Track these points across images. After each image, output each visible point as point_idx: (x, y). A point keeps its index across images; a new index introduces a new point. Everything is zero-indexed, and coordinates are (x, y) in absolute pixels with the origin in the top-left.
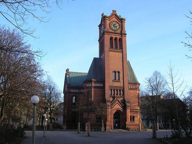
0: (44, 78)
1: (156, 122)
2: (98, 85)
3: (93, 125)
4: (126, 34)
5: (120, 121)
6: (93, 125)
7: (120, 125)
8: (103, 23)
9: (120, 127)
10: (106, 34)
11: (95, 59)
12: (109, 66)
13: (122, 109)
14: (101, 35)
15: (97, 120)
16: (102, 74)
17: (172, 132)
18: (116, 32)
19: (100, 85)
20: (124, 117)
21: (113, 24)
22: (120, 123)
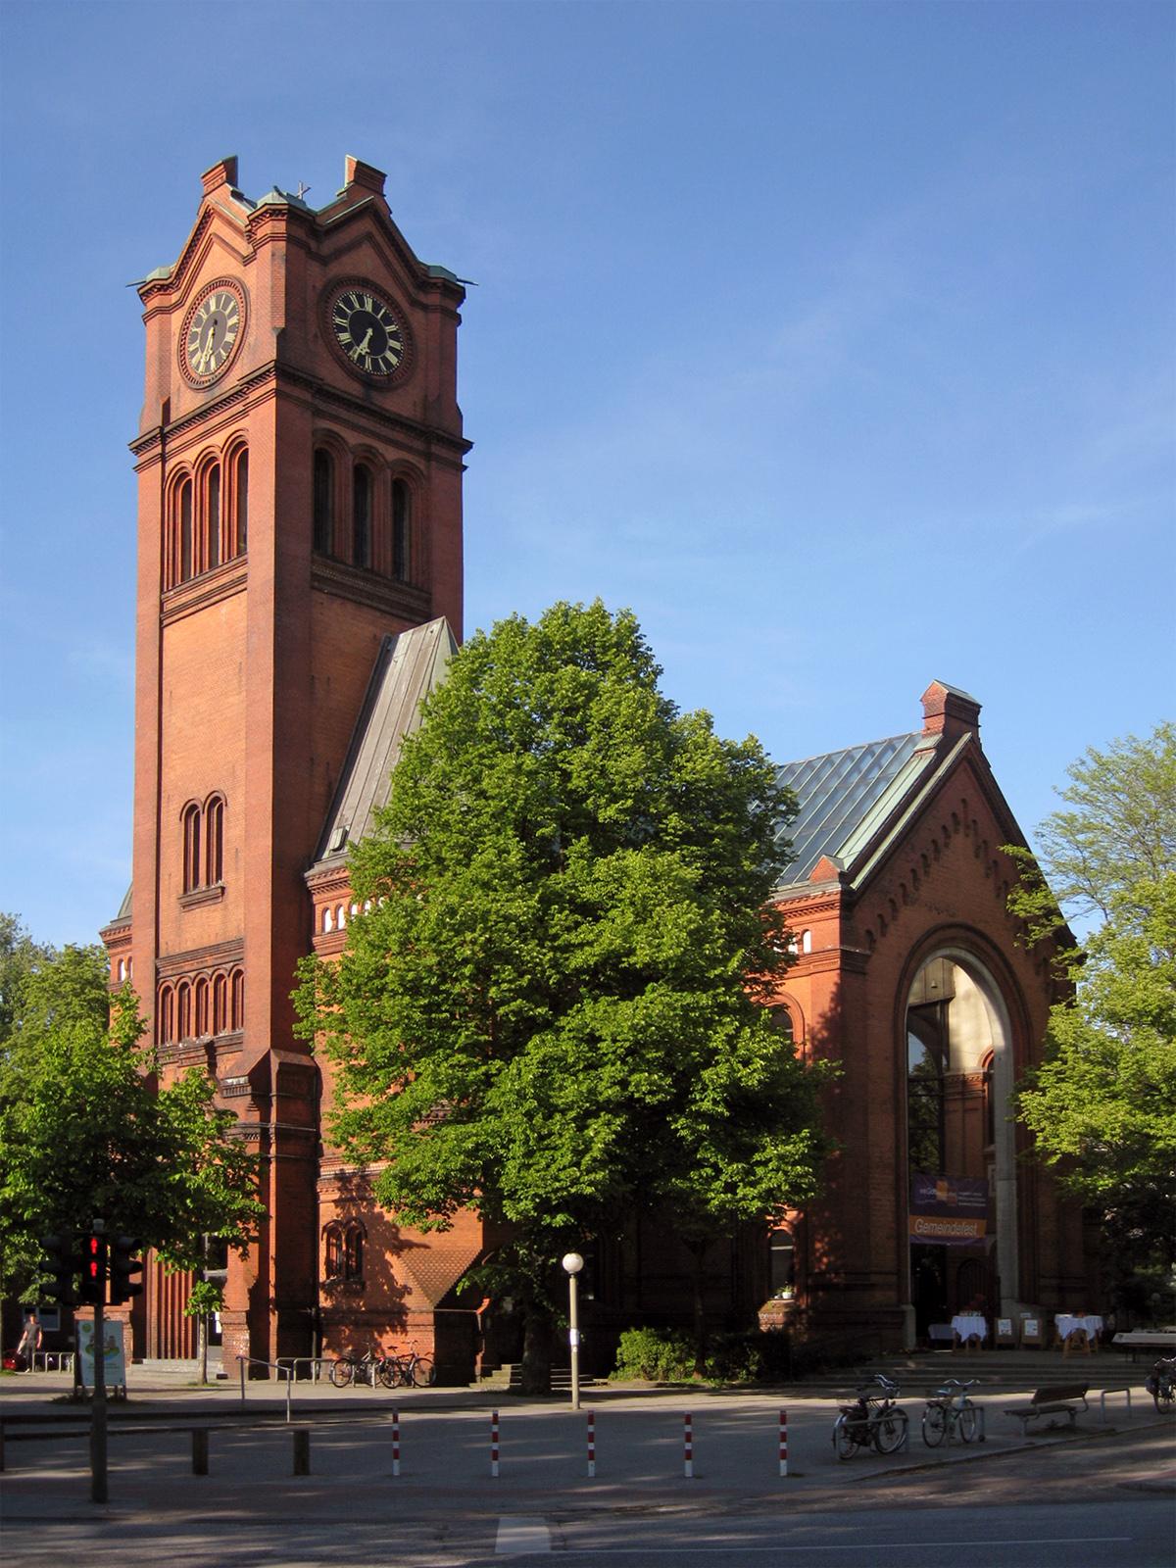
21: (350, 305)
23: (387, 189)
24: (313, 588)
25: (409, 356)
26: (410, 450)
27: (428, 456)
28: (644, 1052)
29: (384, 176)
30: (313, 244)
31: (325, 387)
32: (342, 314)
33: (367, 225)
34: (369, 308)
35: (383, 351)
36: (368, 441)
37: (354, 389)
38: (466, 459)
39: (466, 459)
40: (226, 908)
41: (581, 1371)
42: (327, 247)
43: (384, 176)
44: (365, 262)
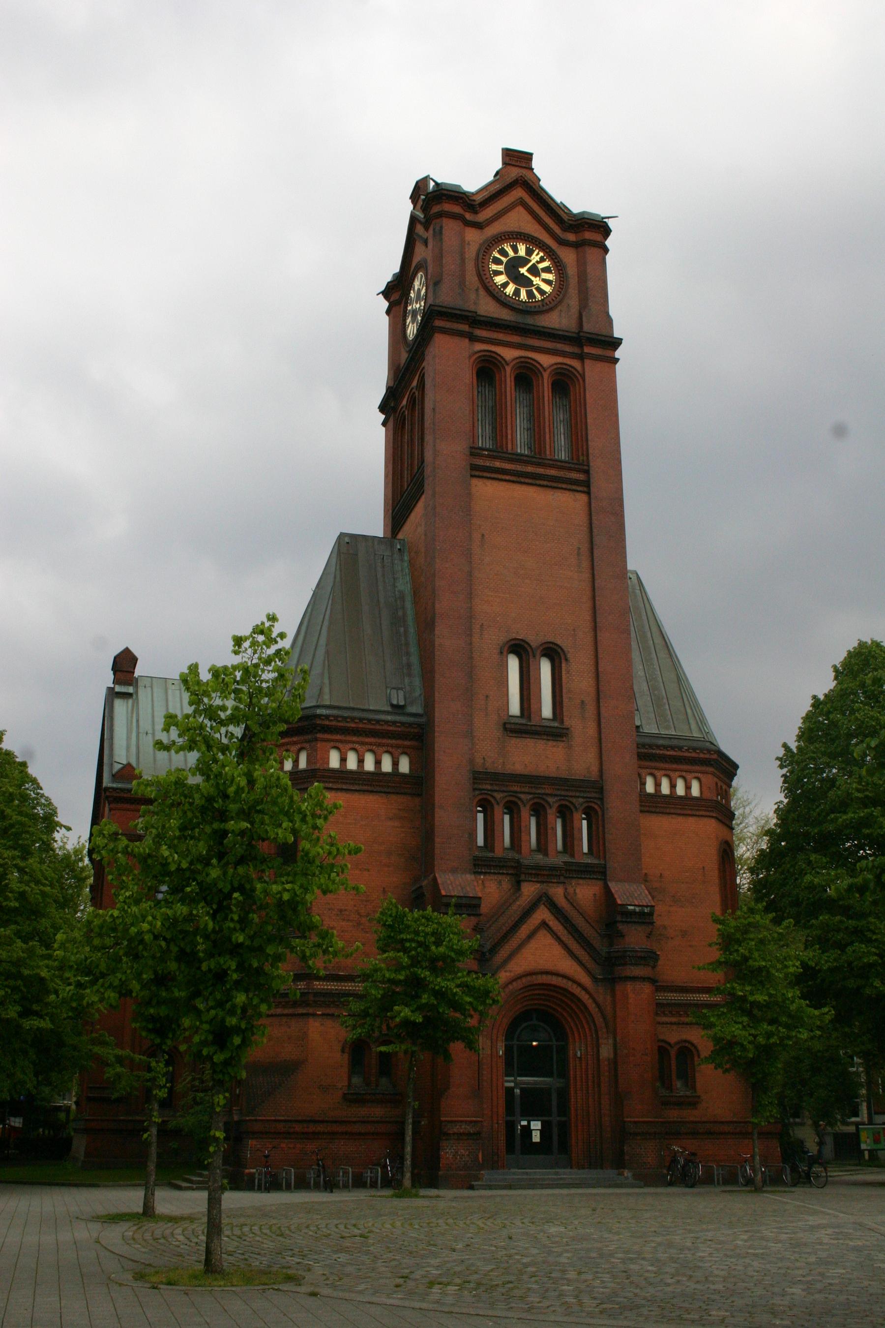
0: (781, 797)
1: (492, 784)
2: (680, 791)
3: (320, 1128)
4: (617, 343)
5: (563, 1093)
6: (320, 1128)
7: (564, 1128)
8: (420, 252)
9: (564, 1147)
10: (444, 331)
11: (349, 548)
12: (470, 596)
13: (585, 980)
14: (404, 356)
15: (356, 1080)
16: (409, 665)
17: (719, 930)
18: (529, 320)
19: (680, 791)
20: (606, 1052)
21: (504, 253)
22: (564, 1108)
23: (534, 164)
24: (472, 476)
25: (561, 284)
26: (563, 354)
27: (581, 357)
28: (195, 780)
29: (531, 154)
30: (468, 216)
31: (478, 318)
32: (498, 262)
33: (519, 193)
34: (511, 254)
35: (508, 276)
36: (560, 360)
37: (505, 315)
38: (618, 354)
39: (618, 354)
40: (570, 747)
41: (159, 1166)
42: (483, 216)
43: (531, 154)
44: (518, 220)
